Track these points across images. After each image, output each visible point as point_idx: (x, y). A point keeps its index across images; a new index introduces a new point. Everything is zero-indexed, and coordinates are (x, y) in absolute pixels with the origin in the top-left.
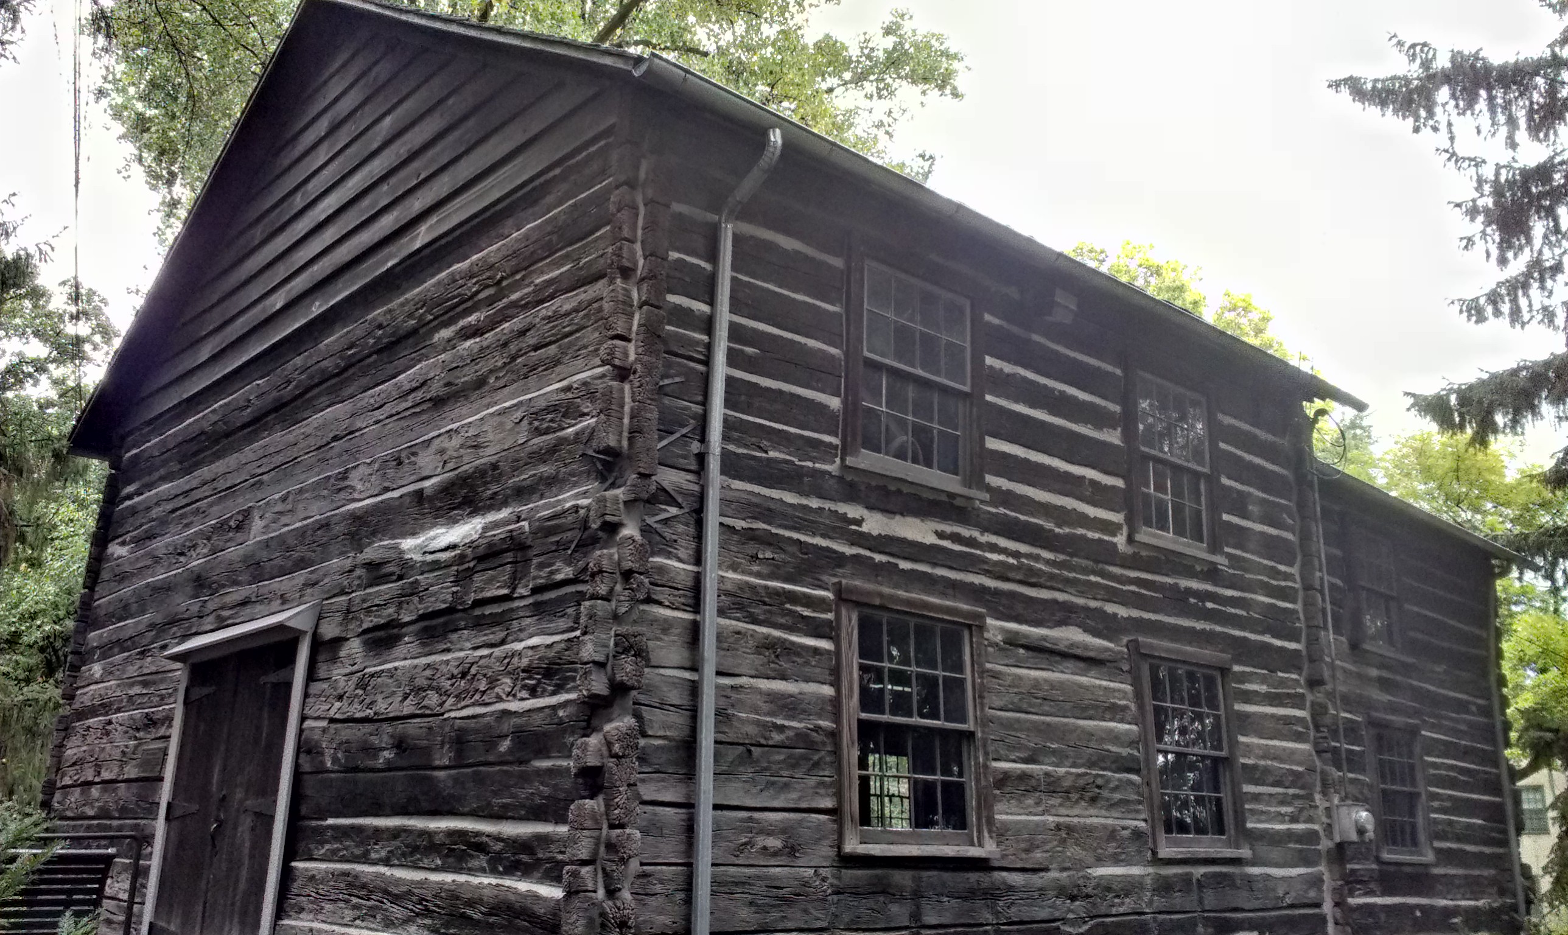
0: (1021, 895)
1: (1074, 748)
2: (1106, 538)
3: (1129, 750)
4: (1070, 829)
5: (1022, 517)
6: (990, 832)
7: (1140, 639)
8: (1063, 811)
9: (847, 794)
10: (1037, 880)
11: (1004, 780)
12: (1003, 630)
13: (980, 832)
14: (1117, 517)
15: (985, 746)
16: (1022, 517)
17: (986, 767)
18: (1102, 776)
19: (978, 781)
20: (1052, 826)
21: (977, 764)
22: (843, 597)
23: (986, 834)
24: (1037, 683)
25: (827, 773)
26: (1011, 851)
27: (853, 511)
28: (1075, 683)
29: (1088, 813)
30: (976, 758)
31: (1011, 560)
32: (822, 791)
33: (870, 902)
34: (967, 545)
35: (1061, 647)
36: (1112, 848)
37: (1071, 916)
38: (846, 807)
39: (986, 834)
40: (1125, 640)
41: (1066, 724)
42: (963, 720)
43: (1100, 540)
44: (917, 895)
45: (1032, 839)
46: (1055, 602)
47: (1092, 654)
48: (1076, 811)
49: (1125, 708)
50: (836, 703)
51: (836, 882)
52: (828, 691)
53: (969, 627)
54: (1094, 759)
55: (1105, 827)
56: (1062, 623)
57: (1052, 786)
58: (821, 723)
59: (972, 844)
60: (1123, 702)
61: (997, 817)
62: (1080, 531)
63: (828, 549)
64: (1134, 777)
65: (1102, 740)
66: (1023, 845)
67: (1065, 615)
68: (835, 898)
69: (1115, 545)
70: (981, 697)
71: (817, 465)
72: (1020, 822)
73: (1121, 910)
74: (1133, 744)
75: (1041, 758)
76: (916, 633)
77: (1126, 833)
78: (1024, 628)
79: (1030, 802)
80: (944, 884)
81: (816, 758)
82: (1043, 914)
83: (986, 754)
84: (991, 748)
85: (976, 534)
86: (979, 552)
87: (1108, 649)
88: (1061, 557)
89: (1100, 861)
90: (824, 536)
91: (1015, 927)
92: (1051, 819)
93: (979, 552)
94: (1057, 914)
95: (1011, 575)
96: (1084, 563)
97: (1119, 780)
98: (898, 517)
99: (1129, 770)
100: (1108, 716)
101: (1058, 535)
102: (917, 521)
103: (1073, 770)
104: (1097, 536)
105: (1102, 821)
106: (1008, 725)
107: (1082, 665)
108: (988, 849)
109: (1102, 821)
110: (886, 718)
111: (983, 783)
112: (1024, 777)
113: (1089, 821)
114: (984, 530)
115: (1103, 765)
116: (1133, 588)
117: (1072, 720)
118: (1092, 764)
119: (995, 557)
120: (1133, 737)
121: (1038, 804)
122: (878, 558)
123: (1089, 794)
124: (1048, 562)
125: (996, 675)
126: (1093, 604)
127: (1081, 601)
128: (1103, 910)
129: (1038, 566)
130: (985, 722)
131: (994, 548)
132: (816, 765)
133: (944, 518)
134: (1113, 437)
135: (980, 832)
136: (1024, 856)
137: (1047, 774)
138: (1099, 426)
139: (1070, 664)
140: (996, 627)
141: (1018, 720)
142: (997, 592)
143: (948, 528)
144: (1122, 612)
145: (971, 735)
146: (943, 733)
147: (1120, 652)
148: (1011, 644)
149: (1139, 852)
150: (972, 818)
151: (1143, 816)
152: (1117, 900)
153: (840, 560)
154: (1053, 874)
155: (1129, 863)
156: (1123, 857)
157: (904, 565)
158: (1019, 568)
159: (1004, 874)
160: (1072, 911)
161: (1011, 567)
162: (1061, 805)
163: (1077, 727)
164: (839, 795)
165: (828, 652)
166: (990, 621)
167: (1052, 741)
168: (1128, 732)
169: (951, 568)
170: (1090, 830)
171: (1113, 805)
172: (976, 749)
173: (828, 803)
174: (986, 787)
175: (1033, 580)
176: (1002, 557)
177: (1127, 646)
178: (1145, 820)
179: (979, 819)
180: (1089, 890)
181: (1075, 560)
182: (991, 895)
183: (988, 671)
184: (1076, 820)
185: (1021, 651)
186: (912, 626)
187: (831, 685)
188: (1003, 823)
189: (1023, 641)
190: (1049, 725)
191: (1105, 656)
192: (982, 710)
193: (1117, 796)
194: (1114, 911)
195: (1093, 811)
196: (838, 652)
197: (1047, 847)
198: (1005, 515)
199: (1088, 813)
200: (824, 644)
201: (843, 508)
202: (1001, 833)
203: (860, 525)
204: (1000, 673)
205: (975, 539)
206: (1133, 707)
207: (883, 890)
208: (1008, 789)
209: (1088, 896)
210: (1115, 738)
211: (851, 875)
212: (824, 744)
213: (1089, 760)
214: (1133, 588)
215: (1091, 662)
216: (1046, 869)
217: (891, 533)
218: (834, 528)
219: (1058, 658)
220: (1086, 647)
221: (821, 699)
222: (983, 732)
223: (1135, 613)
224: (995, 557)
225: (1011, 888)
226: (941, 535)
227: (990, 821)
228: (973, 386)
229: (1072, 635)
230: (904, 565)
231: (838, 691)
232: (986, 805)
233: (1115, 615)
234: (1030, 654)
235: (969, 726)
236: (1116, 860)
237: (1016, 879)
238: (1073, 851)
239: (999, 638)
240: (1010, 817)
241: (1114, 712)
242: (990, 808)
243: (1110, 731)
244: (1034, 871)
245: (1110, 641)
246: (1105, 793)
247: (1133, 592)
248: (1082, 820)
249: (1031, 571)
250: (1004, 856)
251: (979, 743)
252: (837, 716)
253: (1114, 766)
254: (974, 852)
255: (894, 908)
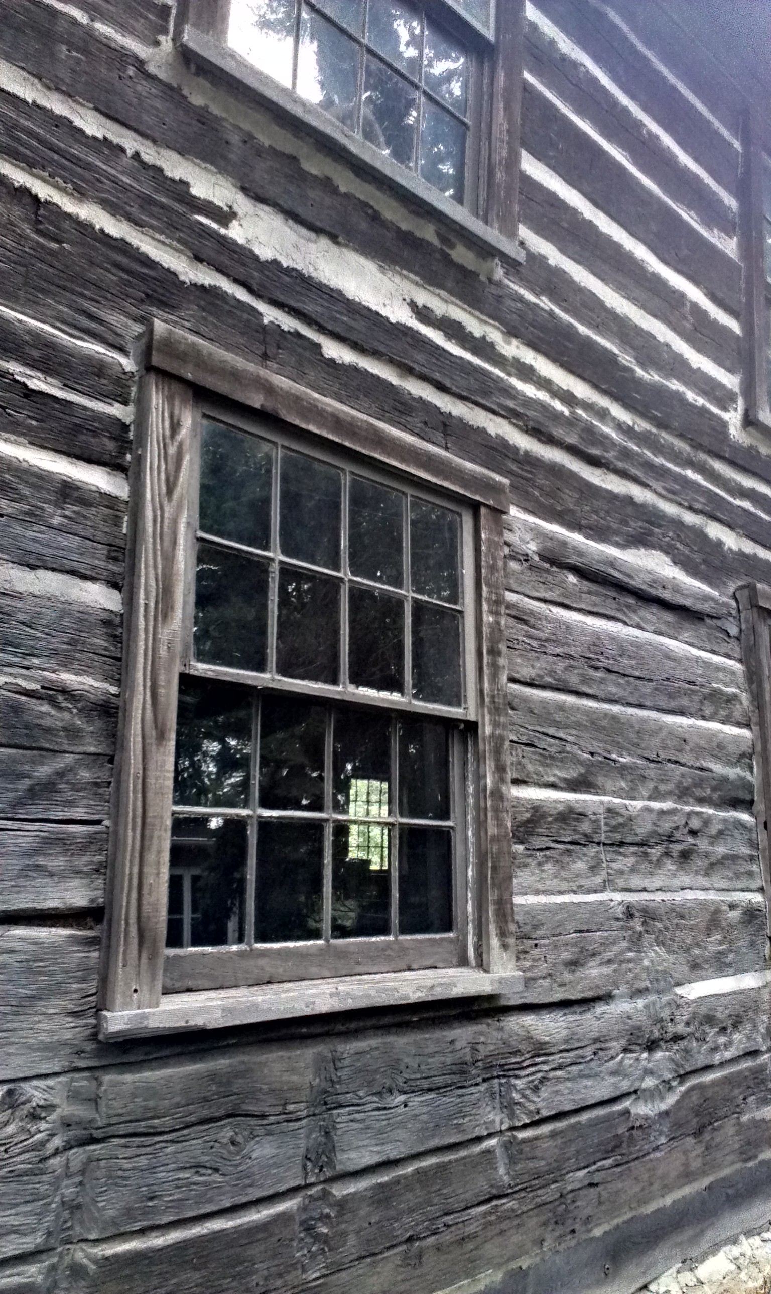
0: (557, 1059)
1: (660, 764)
2: (715, 410)
3: (738, 770)
4: (648, 915)
5: (582, 329)
6: (503, 934)
7: (759, 586)
8: (636, 881)
9: (129, 868)
10: (591, 1022)
11: (533, 822)
12: (538, 534)
13: (481, 933)
14: (731, 381)
15: (498, 752)
16: (582, 329)
17: (498, 795)
18: (698, 814)
19: (481, 825)
20: (620, 911)
21: (481, 790)
22: (160, 367)
23: (495, 942)
24: (597, 642)
25: (79, 813)
26: (543, 968)
27: (207, 186)
28: (659, 648)
29: (677, 882)
30: (480, 777)
31: (558, 405)
32: (57, 862)
33: (195, 1146)
34: (475, 352)
35: (637, 583)
36: (714, 944)
37: (649, 1082)
38: (126, 902)
39: (495, 942)
40: (732, 587)
41: (644, 721)
42: (456, 699)
43: (703, 411)
44: (326, 1101)
45: (582, 939)
46: (629, 500)
47: (688, 602)
48: (657, 882)
49: (732, 699)
50: (118, 628)
51: (80, 1111)
52: (98, 596)
53: (475, 507)
54: (687, 782)
55: (703, 904)
56: (640, 540)
57: (619, 837)
58: (68, 678)
59: (463, 962)
60: (732, 690)
61: (518, 900)
62: (675, 385)
63: (122, 246)
64: (745, 817)
65: (699, 751)
66: (566, 956)
67: (645, 529)
68: (78, 1156)
69: (724, 425)
70: (494, 652)
71: (102, 28)
72: (563, 906)
73: (728, 1055)
74: (744, 758)
75: (600, 780)
76: (354, 501)
77: (735, 915)
78: (576, 538)
79: (580, 866)
80: (395, 1067)
81: (44, 771)
82: (602, 1091)
83: (501, 769)
84: (509, 759)
85: (495, 336)
86: (497, 372)
87: (707, 598)
88: (643, 425)
89: (696, 969)
90: (113, 209)
91: (545, 1129)
92: (618, 897)
93: (497, 372)
94: (625, 1085)
95: (558, 432)
96: (680, 445)
97: (725, 821)
98: (324, 242)
99: (736, 803)
100: (708, 711)
101: (639, 382)
102: (370, 266)
103: (656, 805)
104: (701, 401)
105: (701, 895)
106: (544, 715)
107: (668, 617)
108: (501, 974)
109: (701, 895)
110: (268, 678)
111: (492, 830)
112: (569, 816)
113: (678, 897)
114: (512, 332)
115: (698, 792)
116: (746, 505)
117: (653, 715)
118: (683, 794)
119: (529, 390)
120: (744, 748)
121: (594, 868)
122: (270, 314)
123: (674, 846)
124: (620, 426)
125: (521, 618)
126: (690, 518)
127: (670, 509)
128: (701, 1061)
129: (606, 429)
130: (502, 705)
131: (527, 373)
132: (46, 790)
133: (431, 279)
134: (729, 246)
135: (481, 933)
136: (567, 976)
137: (611, 811)
138: (708, 223)
139: (650, 614)
140: (525, 527)
141: (561, 707)
142: (529, 461)
143: (439, 306)
144: (731, 540)
145: (472, 728)
146: (413, 721)
147: (725, 604)
148: (553, 562)
149: (753, 944)
150: (466, 906)
151: (758, 883)
152: (722, 1040)
153: (162, 289)
154: (621, 1007)
155: (739, 969)
156: (731, 957)
157: (333, 350)
158: (572, 422)
159: (528, 1020)
160: (648, 1072)
161: (557, 417)
162: (633, 870)
163: (661, 728)
164: (107, 870)
165: (110, 501)
166: (514, 511)
167: (621, 749)
168: (736, 739)
169: (441, 388)
170: (679, 913)
171: (713, 866)
172: (479, 758)
173: (77, 895)
174: (496, 839)
175: (595, 451)
176: (542, 396)
177: (734, 597)
178: (761, 890)
179: (480, 907)
180: (680, 1029)
181: (666, 437)
182: (500, 1068)
183: (509, 606)
184: (658, 897)
185: (572, 579)
186: (346, 481)
187: (115, 585)
188: (529, 911)
189: (573, 560)
190: (614, 718)
191: (706, 607)
192: (495, 676)
193: (721, 850)
194: (717, 1058)
195: (686, 880)
196: (135, 504)
197: (609, 955)
198: (551, 314)
199: (677, 882)
200: (96, 478)
201: (177, 167)
202: (523, 936)
203: (226, 225)
204: (532, 613)
205: (492, 345)
206: (745, 697)
207: (232, 1109)
208: (538, 842)
209: (677, 1038)
210: (718, 749)
211: (126, 1084)
212: (73, 733)
213: (679, 785)
214: (746, 505)
215: (685, 614)
216: (607, 997)
217: (309, 271)
218: (147, 202)
219: (631, 601)
220: (677, 589)
221: (83, 618)
222: (496, 725)
223: (749, 547)
224: (529, 390)
225: (540, 1050)
226: (423, 314)
227: (504, 910)
228: (498, 30)
229: (651, 564)
230: (333, 350)
231: (130, 602)
232: (496, 878)
233: (720, 544)
234: (586, 585)
235: (467, 711)
236: (721, 965)
237: (549, 1027)
238: (654, 956)
239: (532, 547)
240: (543, 899)
241: (716, 703)
242: (504, 884)
243: (711, 736)
244: (586, 1002)
245: (710, 584)
246: (703, 844)
247: (745, 511)
248: (667, 896)
249: (589, 432)
250: (529, 982)
251: (486, 747)
252: (118, 666)
253: (715, 796)
254: (466, 982)
255: (263, 1150)
